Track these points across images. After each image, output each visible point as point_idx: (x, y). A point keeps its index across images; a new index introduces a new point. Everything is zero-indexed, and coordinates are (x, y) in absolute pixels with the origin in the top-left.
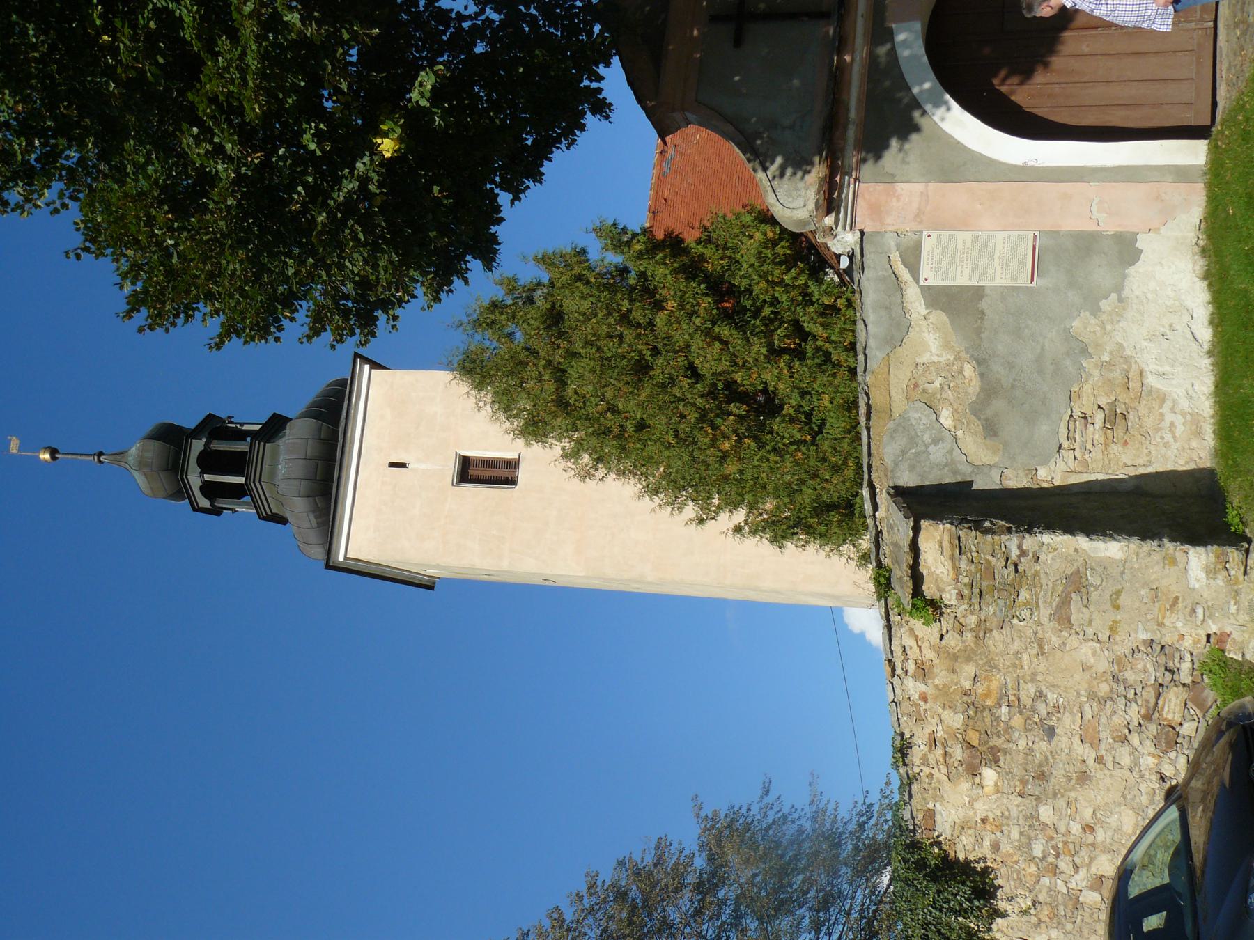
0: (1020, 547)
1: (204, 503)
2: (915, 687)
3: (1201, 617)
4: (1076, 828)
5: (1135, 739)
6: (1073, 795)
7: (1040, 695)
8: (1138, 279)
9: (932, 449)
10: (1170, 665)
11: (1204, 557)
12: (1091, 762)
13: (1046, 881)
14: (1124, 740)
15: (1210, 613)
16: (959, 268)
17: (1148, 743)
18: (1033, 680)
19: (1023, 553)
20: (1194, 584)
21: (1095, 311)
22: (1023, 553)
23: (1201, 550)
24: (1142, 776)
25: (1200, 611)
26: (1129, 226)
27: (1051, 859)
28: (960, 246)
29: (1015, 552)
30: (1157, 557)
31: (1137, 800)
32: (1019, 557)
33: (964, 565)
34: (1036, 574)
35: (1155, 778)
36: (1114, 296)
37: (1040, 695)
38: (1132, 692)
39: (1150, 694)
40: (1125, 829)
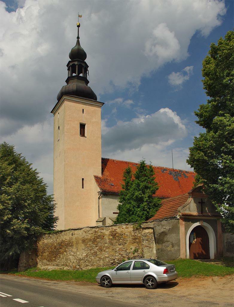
4: (105, 249)
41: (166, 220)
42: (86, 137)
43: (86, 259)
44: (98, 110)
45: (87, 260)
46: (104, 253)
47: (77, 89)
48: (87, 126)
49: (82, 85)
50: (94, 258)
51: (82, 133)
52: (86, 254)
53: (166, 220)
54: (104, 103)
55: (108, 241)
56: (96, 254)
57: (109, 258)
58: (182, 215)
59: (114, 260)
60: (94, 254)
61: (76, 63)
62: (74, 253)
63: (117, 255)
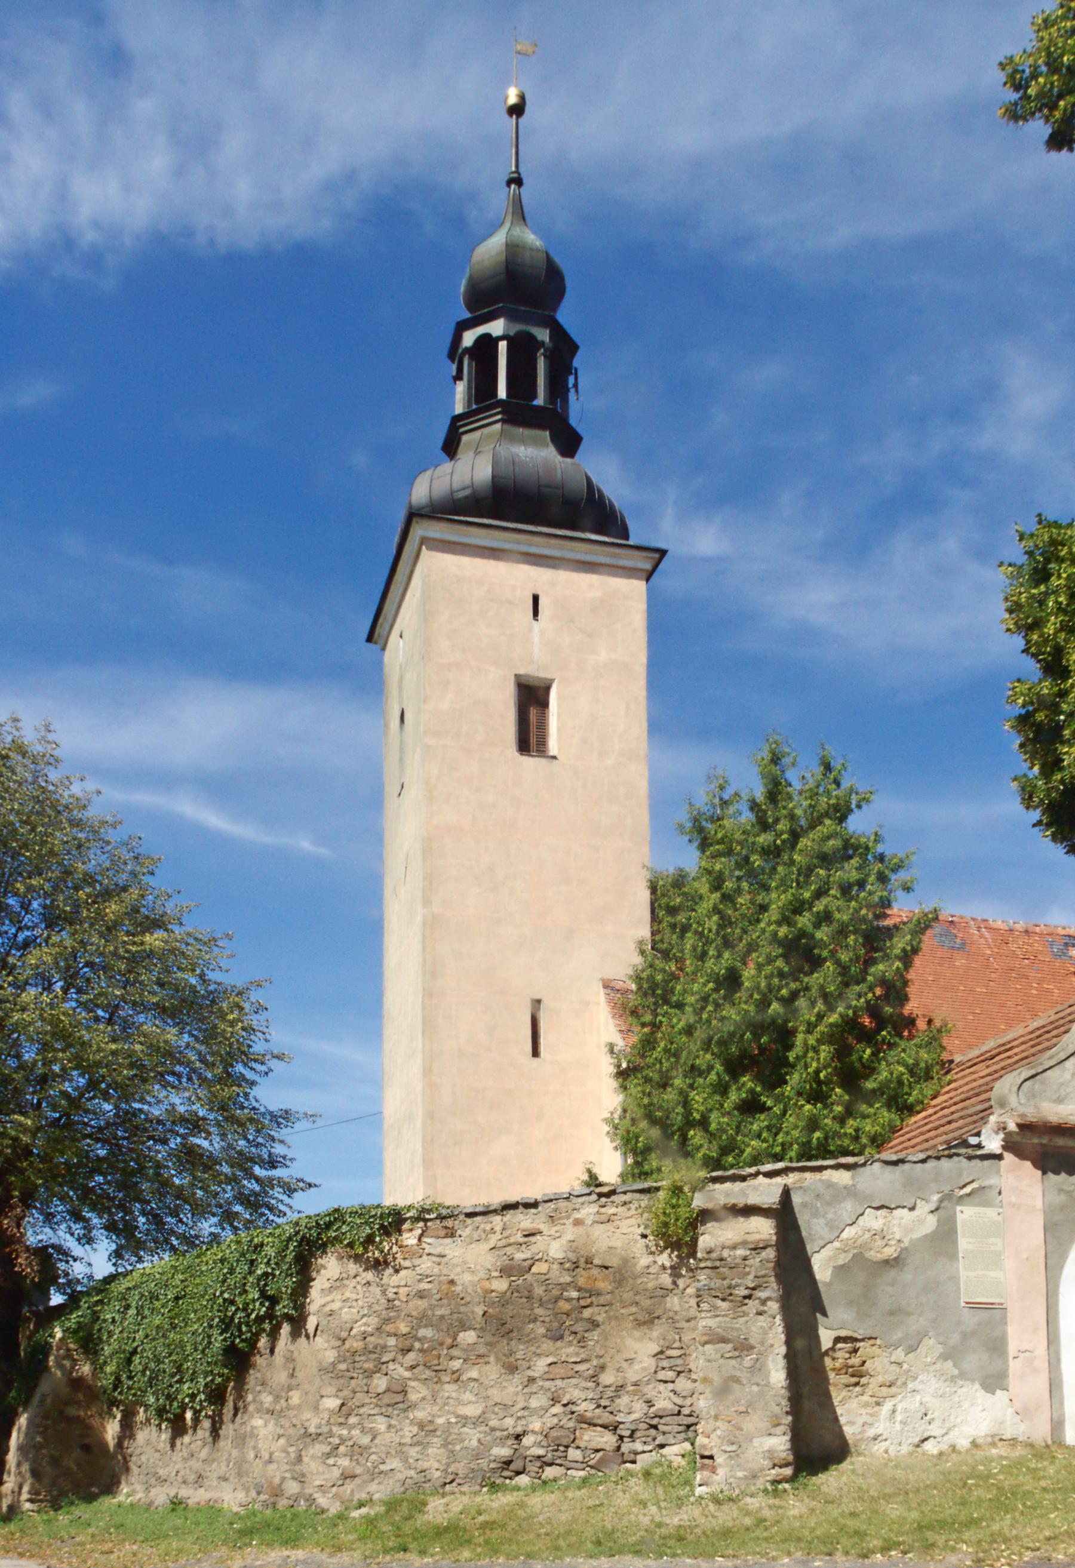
0: (769, 1299)
1: (469, 338)
2: (589, 1214)
3: (729, 1449)
4: (456, 1364)
5: (557, 1409)
6: (492, 1359)
7: (595, 1324)
8: (973, 1391)
9: (822, 1221)
10: (638, 1434)
11: (783, 1448)
12: (530, 1373)
13: (392, 1342)
14: (555, 1400)
15: (733, 1455)
16: (973, 1240)
17: (555, 1420)
18: (610, 1318)
19: (764, 1302)
20: (756, 1442)
21: (945, 1357)
22: (764, 1302)
23: (788, 1446)
24: (519, 1418)
25: (734, 1448)
26: (1012, 1381)
27: (417, 1345)
28: (992, 1240)
29: (763, 1295)
30: (777, 1410)
31: (493, 1416)
32: (759, 1298)
33: (740, 1252)
34: (745, 1314)
35: (519, 1430)
36: (956, 1372)
37: (595, 1324)
38: (607, 1404)
39: (606, 1418)
40: (460, 1407)
41: (895, 1163)
42: (554, 758)
43: (340, 1436)
44: (631, 594)
45: (343, 1441)
46: (450, 1389)
47: (493, 477)
48: (560, 697)
49: (534, 454)
50: (390, 1426)
51: (530, 739)
52: (339, 1402)
53: (895, 1163)
54: (663, 553)
55: (479, 1311)
56: (399, 1398)
57: (483, 1428)
58: (1019, 1125)
59: (518, 1437)
60: (387, 1399)
61: (496, 327)
62: (277, 1398)
63: (534, 1403)
